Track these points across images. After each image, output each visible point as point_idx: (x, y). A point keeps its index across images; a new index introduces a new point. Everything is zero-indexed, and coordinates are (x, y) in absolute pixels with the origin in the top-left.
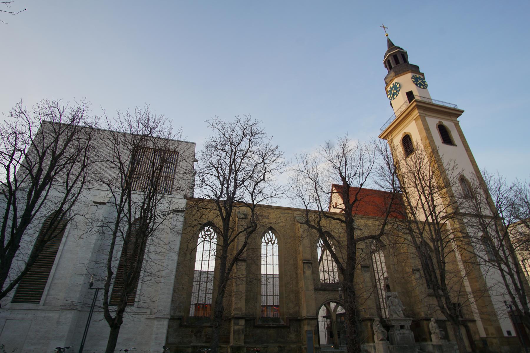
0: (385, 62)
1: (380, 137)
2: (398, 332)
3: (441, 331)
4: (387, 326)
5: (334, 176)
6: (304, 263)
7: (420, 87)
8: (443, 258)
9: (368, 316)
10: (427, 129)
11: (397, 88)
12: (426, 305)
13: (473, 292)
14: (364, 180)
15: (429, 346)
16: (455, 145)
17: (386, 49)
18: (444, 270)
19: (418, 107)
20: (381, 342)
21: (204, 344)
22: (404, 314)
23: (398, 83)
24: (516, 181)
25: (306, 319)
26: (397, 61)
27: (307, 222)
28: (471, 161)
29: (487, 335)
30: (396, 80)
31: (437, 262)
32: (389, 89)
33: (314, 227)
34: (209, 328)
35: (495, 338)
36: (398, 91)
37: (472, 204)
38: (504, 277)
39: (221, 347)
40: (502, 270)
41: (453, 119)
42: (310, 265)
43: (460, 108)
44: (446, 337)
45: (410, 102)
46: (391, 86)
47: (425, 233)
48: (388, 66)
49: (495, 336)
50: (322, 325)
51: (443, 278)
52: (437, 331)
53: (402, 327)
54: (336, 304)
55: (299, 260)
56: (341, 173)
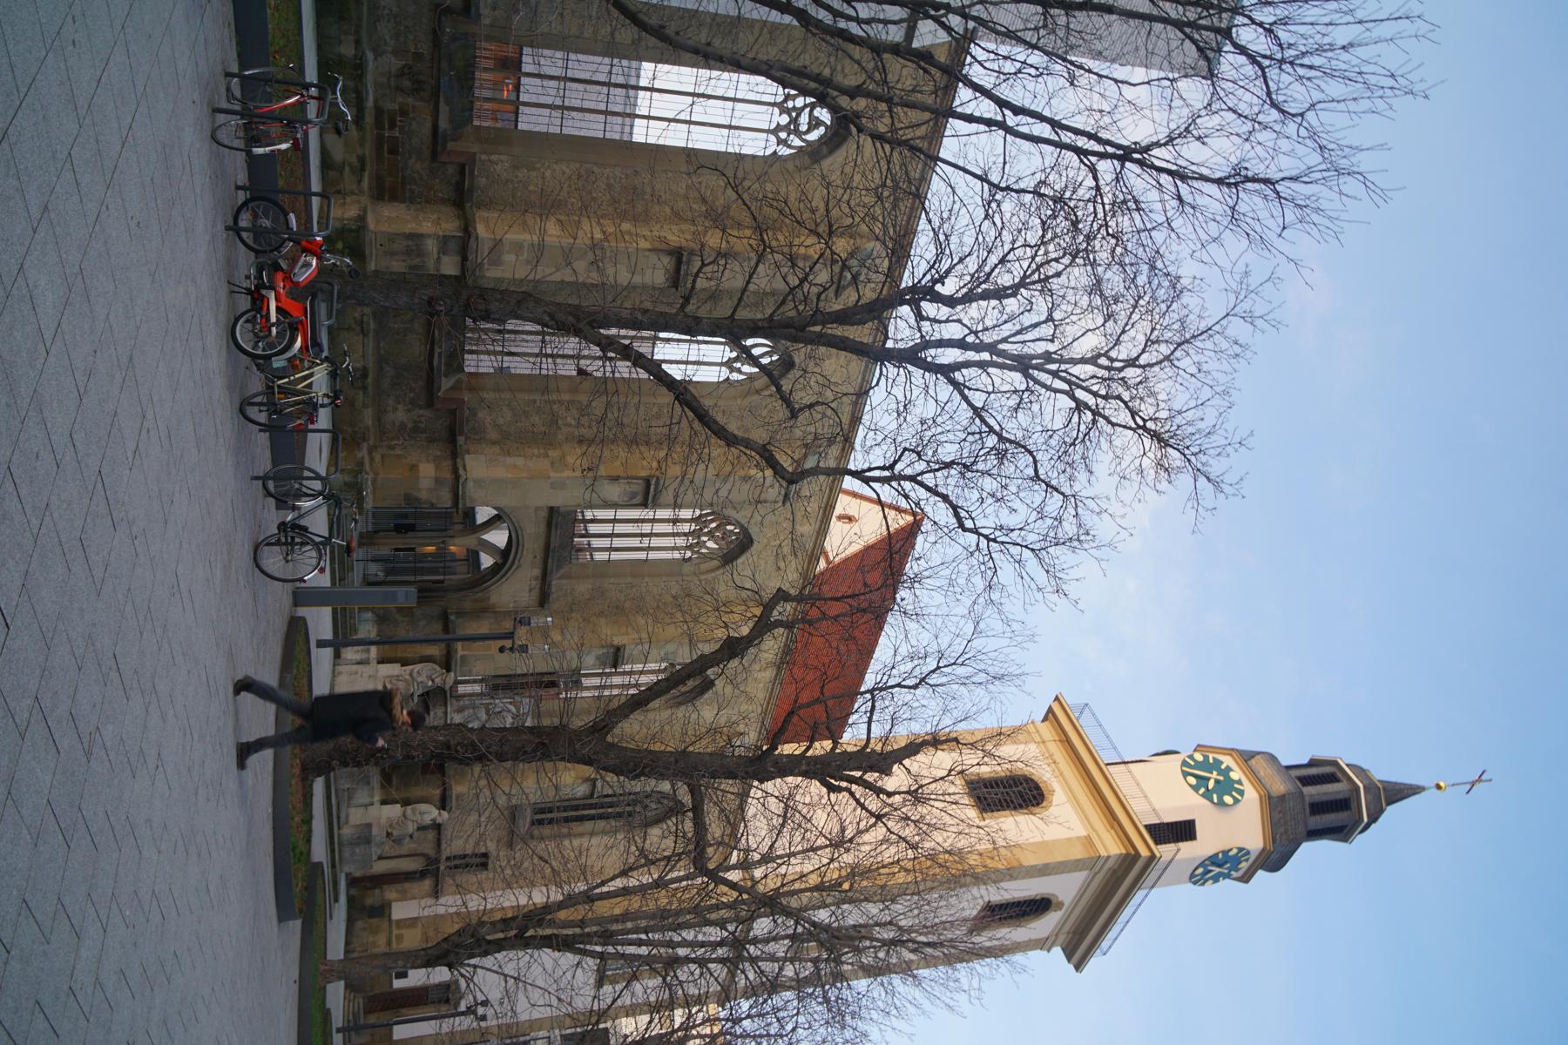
0: (1335, 763)
1: (1057, 699)
7: (1201, 865)
10: (1044, 870)
11: (1220, 791)
17: (1381, 773)
21: (370, 103)
23: (1236, 801)
25: (455, 471)
26: (1323, 804)
29: (399, 922)
30: (1251, 794)
32: (1227, 761)
34: (429, 125)
35: (389, 943)
36: (1207, 795)
39: (363, 169)
41: (1062, 938)
43: (1095, 962)
46: (1235, 775)
48: (1314, 771)
49: (394, 946)
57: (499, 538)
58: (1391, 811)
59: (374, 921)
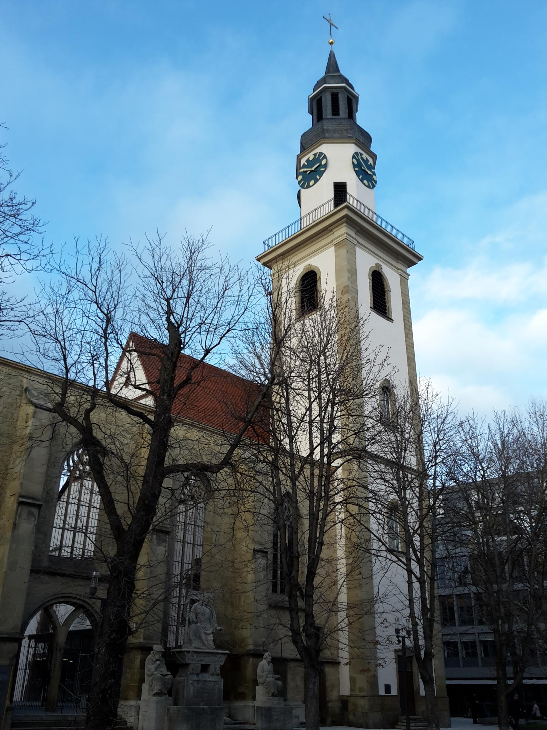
1: (258, 260)
2: (195, 678)
3: (277, 679)
4: (174, 662)
5: (153, 315)
6: (20, 503)
8: (323, 532)
9: (141, 640)
12: (260, 624)
13: (350, 606)
14: (215, 343)
15: (247, 710)
16: (390, 320)
18: (318, 556)
19: (349, 221)
20: (155, 698)
22: (214, 641)
23: (325, 157)
24: (471, 415)
26: (334, 107)
27: (60, 408)
28: (408, 357)
29: (352, 690)
31: (310, 540)
33: (72, 421)
37: (393, 439)
38: (410, 583)
40: (410, 572)
41: (400, 266)
42: (35, 511)
43: (418, 249)
44: (281, 693)
45: (336, 206)
47: (301, 479)
48: (315, 112)
50: (26, 652)
51: (312, 574)
52: (270, 679)
53: (205, 668)
54: (71, 608)
55: (8, 493)
56: (170, 312)
57: (63, 611)
58: (344, 71)
59: (350, 707)
